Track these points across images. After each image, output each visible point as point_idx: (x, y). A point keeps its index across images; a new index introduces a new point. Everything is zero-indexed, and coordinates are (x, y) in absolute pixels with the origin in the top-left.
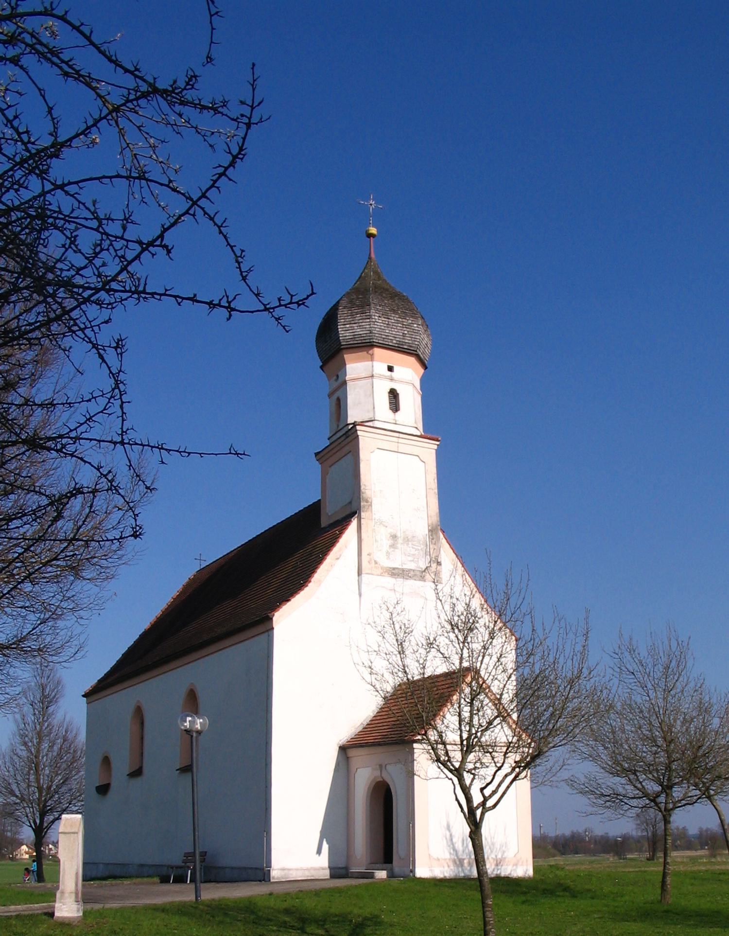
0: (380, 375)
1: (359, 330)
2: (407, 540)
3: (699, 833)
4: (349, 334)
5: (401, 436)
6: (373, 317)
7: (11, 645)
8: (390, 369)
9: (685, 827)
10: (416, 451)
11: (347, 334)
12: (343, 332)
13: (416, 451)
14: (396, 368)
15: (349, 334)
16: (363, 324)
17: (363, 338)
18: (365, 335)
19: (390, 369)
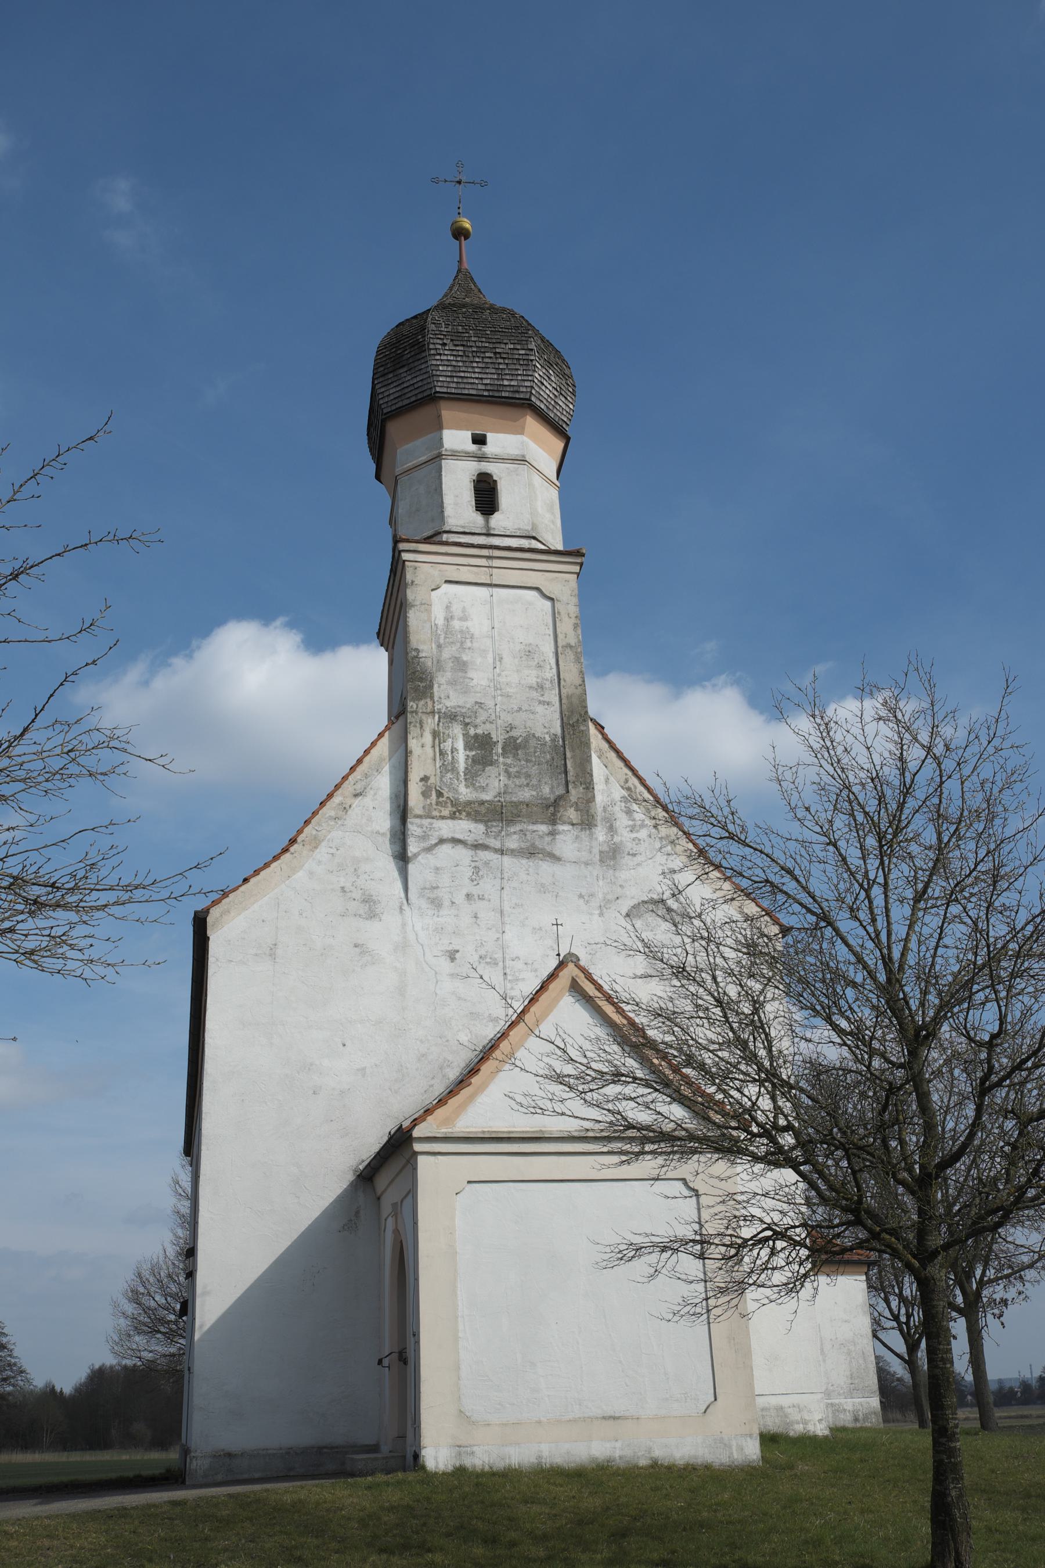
0: (456, 452)
1: (409, 378)
2: (512, 746)
3: (752, 1450)
4: (394, 390)
5: (497, 553)
6: (431, 346)
7: (981, 1218)
8: (479, 440)
9: (196, 913)
10: (533, 579)
11: (391, 391)
12: (383, 390)
13: (533, 579)
14: (490, 437)
15: (394, 390)
16: (416, 364)
17: (417, 392)
18: (420, 384)
19: (479, 440)
